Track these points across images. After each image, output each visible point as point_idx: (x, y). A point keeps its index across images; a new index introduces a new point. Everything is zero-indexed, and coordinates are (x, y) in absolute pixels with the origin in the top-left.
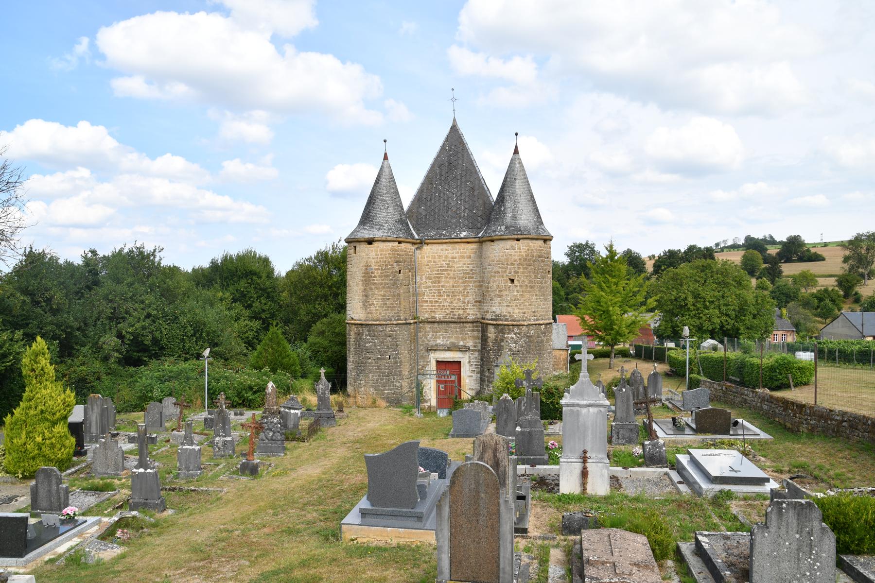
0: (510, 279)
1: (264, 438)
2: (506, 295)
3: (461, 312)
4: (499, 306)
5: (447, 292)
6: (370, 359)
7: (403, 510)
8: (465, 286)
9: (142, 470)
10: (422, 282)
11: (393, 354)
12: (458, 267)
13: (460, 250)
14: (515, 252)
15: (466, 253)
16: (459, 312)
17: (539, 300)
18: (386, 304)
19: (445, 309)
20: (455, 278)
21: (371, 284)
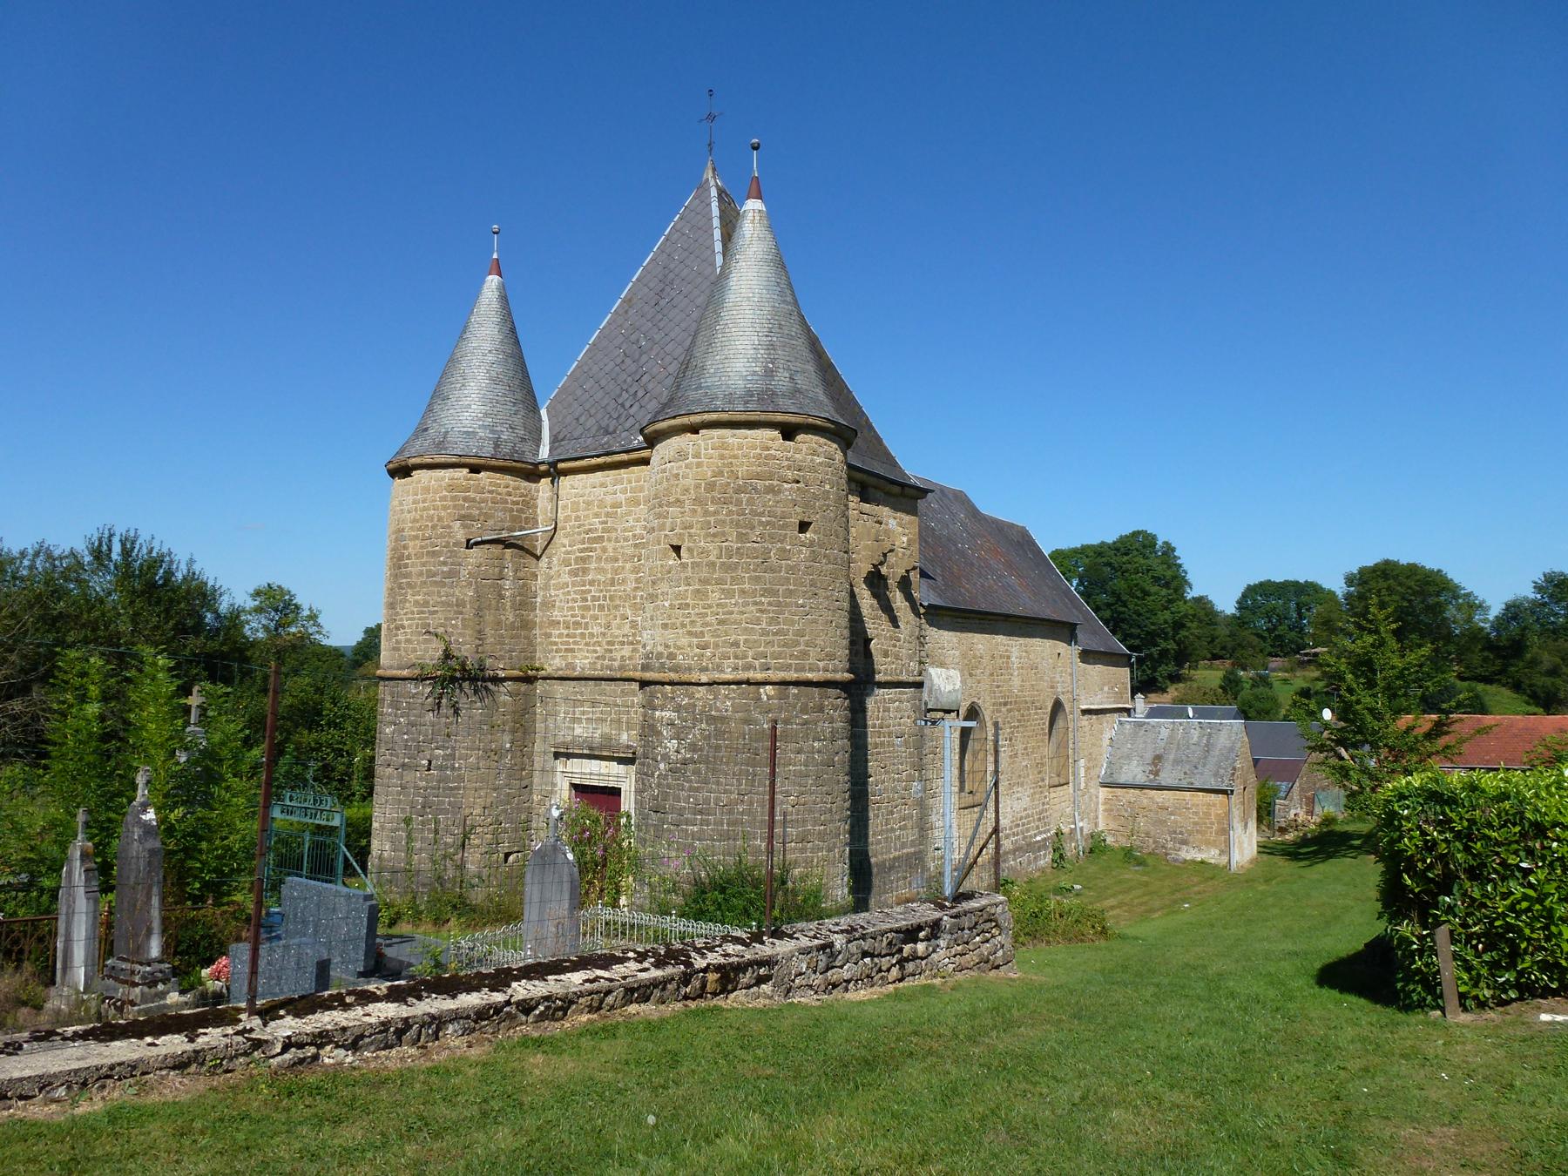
0: (672, 546)
10: (552, 572)
11: (437, 758)
12: (625, 530)
13: (630, 482)
17: (753, 608)
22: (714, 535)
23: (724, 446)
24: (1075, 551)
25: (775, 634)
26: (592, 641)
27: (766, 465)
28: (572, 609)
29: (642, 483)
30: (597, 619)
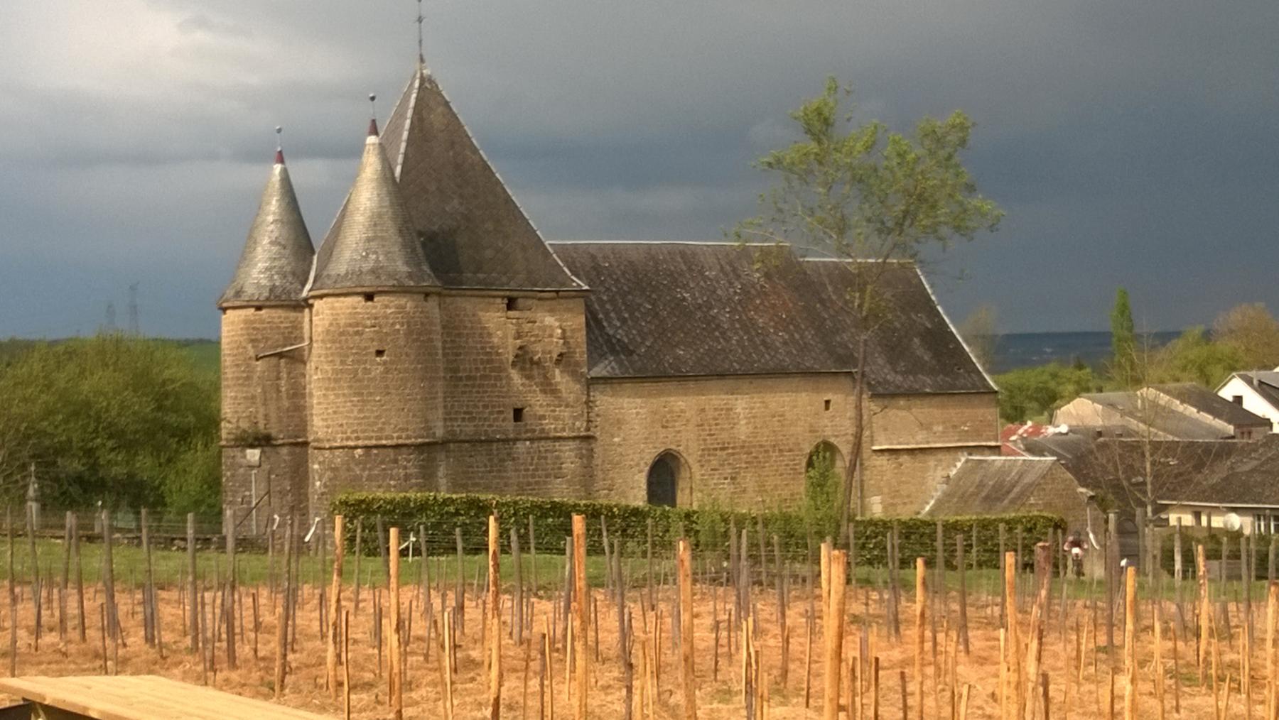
17: (349, 404)
23: (333, 308)
25: (362, 418)
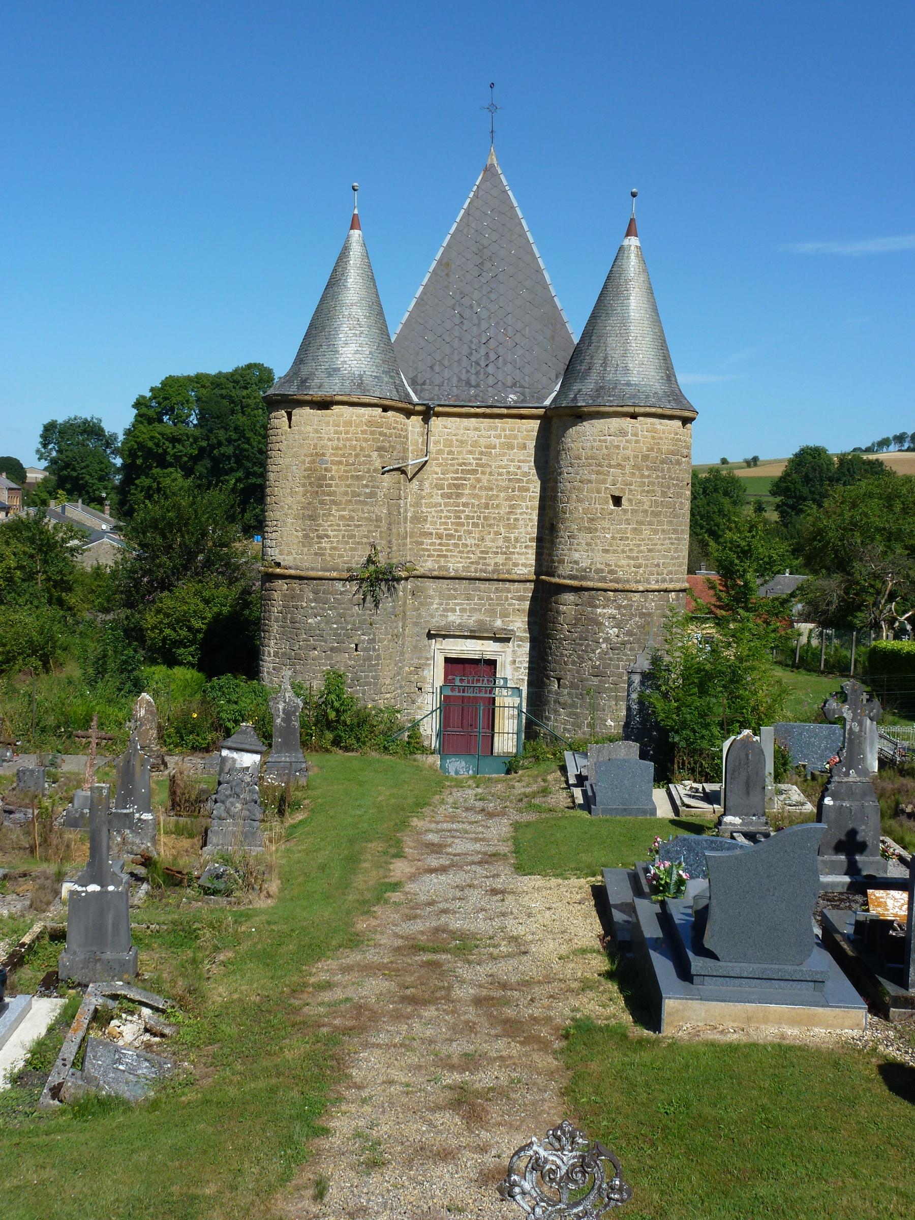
1: (224, 815)
2: (604, 528)
3: (500, 559)
4: (587, 551)
5: (473, 518)
6: (315, 649)
7: (786, 967)
8: (511, 506)
9: (94, 888)
10: (424, 493)
12: (500, 467)
14: (627, 441)
15: (515, 437)
16: (497, 560)
17: (667, 541)
18: (353, 536)
19: (468, 552)
20: (492, 489)
21: (324, 493)
22: (648, 492)
24: (189, 379)
26: (466, 550)
27: (676, 445)
28: (446, 523)
29: (516, 432)
30: (471, 533)
